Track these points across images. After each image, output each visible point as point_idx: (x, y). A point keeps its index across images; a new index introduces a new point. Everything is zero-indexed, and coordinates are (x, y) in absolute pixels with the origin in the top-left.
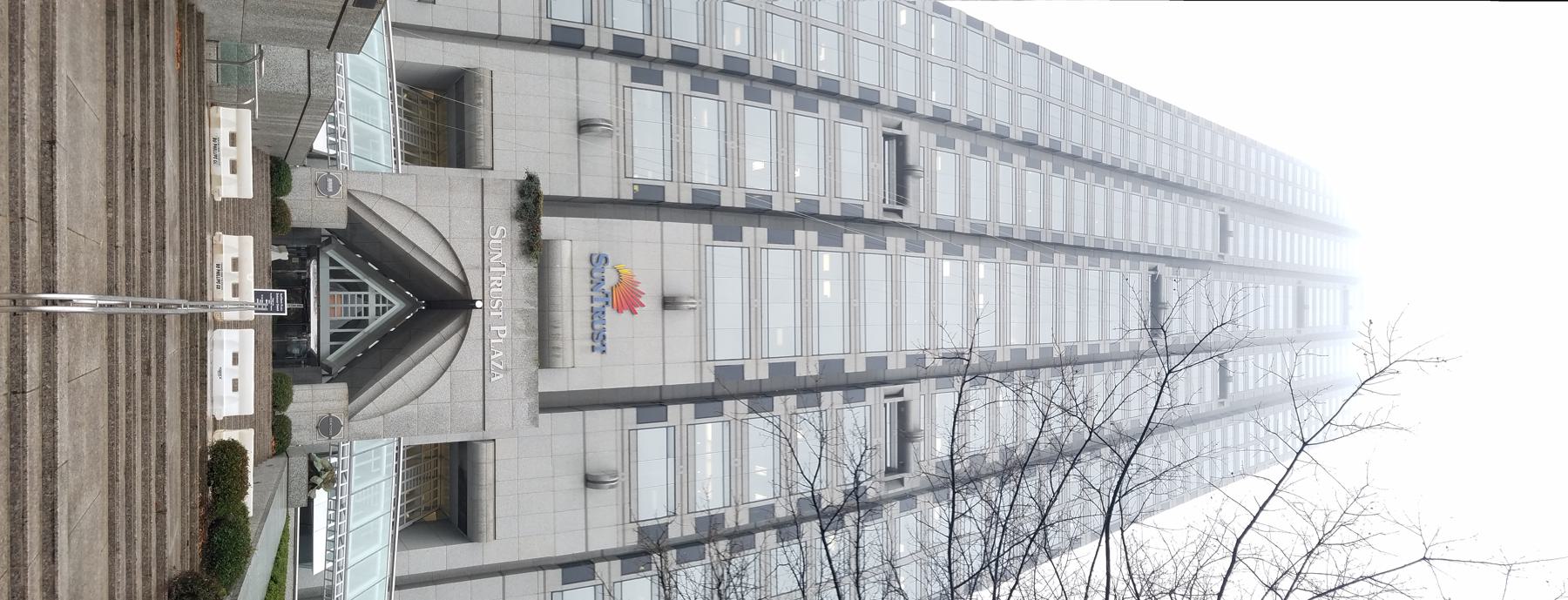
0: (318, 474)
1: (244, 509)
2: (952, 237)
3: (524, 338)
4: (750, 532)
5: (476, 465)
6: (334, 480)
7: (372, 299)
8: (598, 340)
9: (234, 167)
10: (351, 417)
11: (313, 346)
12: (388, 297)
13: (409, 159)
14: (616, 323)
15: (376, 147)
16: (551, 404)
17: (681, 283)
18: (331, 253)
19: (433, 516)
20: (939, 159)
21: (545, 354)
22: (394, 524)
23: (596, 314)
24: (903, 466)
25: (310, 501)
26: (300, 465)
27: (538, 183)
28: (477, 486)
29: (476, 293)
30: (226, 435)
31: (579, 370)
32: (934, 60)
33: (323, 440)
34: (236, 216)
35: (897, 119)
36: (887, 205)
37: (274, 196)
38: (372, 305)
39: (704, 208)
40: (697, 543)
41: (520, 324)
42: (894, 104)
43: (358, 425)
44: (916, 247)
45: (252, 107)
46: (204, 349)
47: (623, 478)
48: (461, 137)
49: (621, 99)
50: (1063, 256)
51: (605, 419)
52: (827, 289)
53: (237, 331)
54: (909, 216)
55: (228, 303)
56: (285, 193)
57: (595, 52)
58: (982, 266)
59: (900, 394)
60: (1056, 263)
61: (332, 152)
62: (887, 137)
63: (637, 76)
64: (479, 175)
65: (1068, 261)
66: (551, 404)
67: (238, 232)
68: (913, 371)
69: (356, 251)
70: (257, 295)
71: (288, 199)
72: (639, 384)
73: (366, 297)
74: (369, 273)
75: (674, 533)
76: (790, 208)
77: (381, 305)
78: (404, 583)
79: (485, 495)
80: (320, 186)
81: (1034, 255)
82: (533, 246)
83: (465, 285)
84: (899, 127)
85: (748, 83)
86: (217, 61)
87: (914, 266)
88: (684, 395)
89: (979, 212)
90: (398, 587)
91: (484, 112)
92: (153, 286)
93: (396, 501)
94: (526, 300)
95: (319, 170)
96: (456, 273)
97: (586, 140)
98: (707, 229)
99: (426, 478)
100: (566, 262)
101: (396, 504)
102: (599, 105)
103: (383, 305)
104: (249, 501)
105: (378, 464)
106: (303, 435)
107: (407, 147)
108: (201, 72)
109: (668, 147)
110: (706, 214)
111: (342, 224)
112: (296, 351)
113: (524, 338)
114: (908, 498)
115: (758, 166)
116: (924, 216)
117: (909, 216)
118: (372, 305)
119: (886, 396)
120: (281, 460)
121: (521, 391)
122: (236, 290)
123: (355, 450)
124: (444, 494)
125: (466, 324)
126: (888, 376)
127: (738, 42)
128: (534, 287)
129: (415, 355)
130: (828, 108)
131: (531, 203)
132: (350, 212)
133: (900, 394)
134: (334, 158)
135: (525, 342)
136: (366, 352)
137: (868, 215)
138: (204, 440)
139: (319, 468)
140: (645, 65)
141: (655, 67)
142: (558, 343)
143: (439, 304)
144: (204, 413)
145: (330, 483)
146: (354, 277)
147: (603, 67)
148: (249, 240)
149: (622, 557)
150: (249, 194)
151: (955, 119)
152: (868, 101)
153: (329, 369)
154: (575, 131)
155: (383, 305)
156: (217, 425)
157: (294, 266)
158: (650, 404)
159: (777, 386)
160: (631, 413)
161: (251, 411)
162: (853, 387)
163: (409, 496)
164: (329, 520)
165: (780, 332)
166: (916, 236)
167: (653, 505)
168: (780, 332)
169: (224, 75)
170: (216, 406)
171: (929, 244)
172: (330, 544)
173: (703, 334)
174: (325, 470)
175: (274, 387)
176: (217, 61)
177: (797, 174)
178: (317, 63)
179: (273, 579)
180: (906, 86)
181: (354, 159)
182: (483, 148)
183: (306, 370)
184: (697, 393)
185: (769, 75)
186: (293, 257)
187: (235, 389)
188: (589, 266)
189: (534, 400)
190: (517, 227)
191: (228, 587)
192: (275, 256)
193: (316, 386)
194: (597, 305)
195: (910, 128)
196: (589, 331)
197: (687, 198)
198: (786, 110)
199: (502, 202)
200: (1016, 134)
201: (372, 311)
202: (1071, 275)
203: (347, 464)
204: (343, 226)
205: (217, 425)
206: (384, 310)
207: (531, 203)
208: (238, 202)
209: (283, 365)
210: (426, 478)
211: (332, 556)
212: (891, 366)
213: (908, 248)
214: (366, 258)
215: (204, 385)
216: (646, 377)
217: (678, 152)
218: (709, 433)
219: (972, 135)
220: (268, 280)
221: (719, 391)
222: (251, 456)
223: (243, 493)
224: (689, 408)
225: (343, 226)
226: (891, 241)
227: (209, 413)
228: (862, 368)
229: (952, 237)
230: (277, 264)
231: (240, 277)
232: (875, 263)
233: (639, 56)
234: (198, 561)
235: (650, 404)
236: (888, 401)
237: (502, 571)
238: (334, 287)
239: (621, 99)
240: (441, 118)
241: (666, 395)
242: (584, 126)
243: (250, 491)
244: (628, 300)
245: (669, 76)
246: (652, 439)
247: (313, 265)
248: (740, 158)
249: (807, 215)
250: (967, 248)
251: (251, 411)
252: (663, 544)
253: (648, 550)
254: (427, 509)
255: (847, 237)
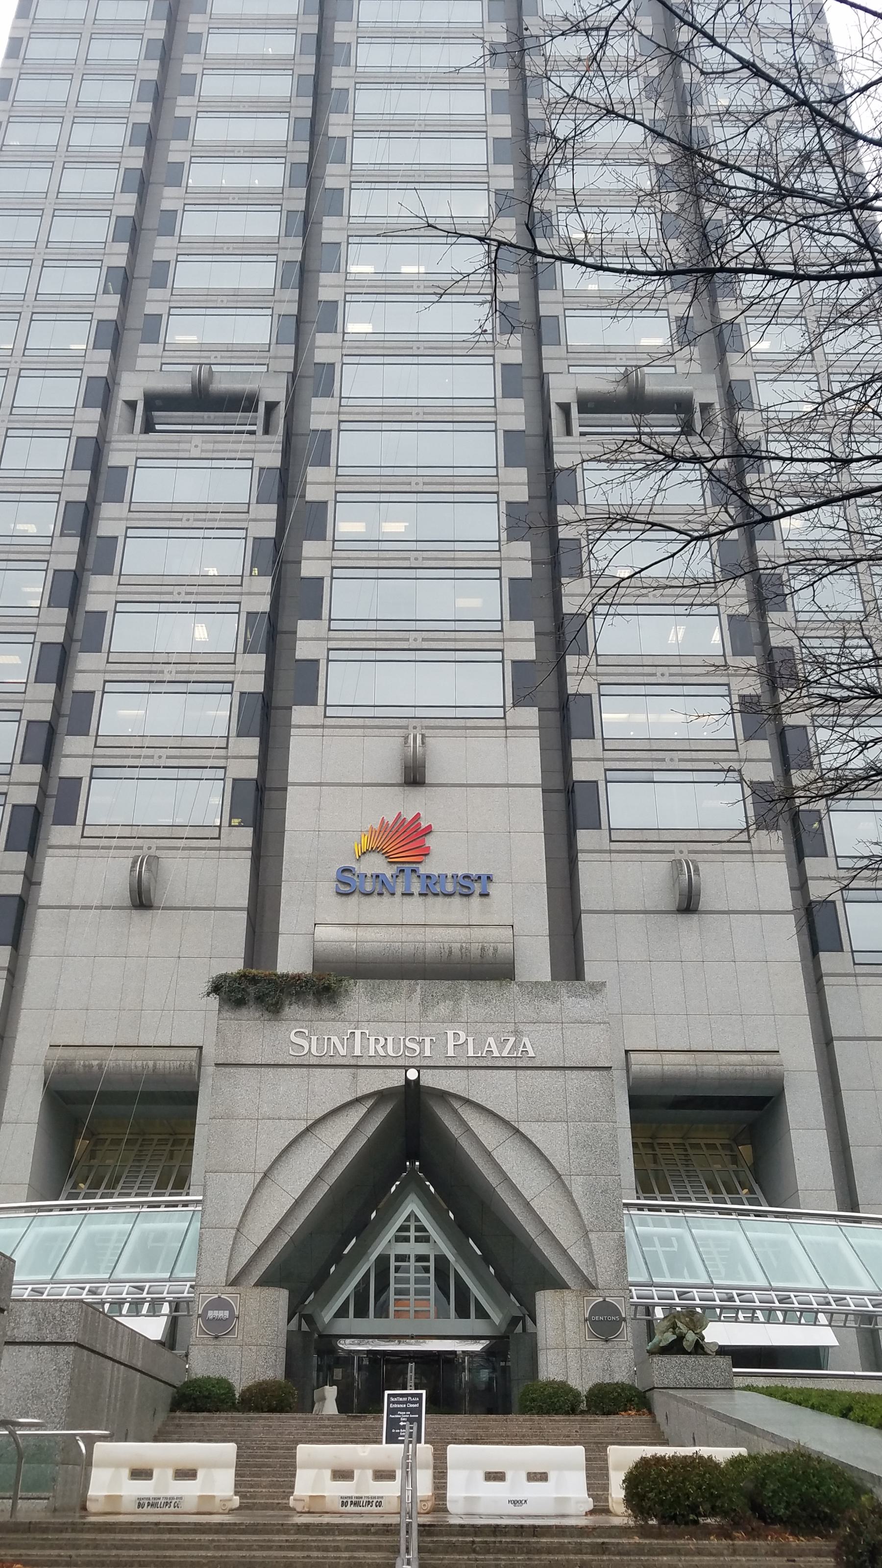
0: (679, 1337)
1: (736, 1462)
2: (307, 317)
3: (466, 1003)
4: (768, 653)
5: (665, 1081)
6: (690, 1312)
7: (402, 1248)
8: (472, 886)
9: (186, 1474)
10: (589, 1286)
11: (477, 1347)
12: (399, 1221)
13: (181, 1183)
14: (445, 858)
15: (161, 1236)
16: (569, 962)
17: (382, 755)
18: (327, 1315)
19: (745, 1151)
20: (180, 339)
21: (491, 971)
22: (758, 1214)
23: (432, 888)
24: (680, 405)
25: (723, 1351)
26: (666, 1370)
27: (224, 977)
28: (697, 1080)
29: (395, 1079)
30: (617, 1492)
31: (518, 918)
32: (20, 345)
33: (628, 1333)
34: (262, 1474)
35: (119, 409)
36: (259, 428)
37: (234, 1408)
38: (412, 1248)
39: (264, 721)
40: (781, 736)
41: (444, 1009)
42: (96, 413)
43: (604, 1276)
44: (325, 379)
45: (90, 1441)
46: (477, 1530)
47: (682, 852)
48: (150, 1097)
49: (101, 841)
50: (334, 118)
51: (595, 879)
52: (394, 528)
53: (451, 1474)
54: (275, 391)
55: (403, 1490)
56: (230, 1388)
57: (31, 879)
58: (353, 269)
59: (565, 408)
60: (346, 132)
61: (166, 1309)
62: (149, 427)
63: (67, 817)
64: (209, 1070)
65: (342, 109)
66: (569, 962)
67: (289, 1469)
68: (530, 386)
69: (324, 1274)
70: (392, 1439)
71: (240, 1383)
72: (542, 828)
73: (400, 1258)
74: (360, 1253)
75: (766, 773)
76: (266, 584)
77: (412, 1234)
78: (849, 1198)
79: (711, 1066)
80: (219, 1330)
81: (333, 176)
82: (323, 986)
83: (381, 1096)
84: (132, 405)
85: (77, 646)
86: (15, 1498)
87: (358, 382)
88: (557, 756)
89: (262, 275)
90: (855, 1207)
91: (114, 1060)
92: (384, 1539)
93: (722, 1211)
94: (406, 1000)
95: (194, 1329)
96: (362, 1110)
97: (161, 897)
98: (300, 714)
99: (687, 1161)
100: (348, 934)
101: (728, 1212)
102: (111, 874)
103: (413, 1229)
104: (722, 1454)
105: (665, 1241)
106: (618, 1363)
107: (161, 1186)
108: (30, 1527)
109: (173, 773)
110: (277, 716)
111: (280, 1297)
112: (484, 1375)
113: (466, 1003)
114: (735, 398)
115: (201, 633)
116: (275, 365)
117: (275, 391)
118: (412, 1248)
119: (569, 432)
120: (658, 1399)
121: (550, 1009)
122: (383, 1475)
123: (644, 1278)
124: (709, 1133)
125: (443, 1096)
126: (537, 429)
127: (15, 660)
128: (387, 986)
129: (492, 1179)
130: (110, 521)
131: (254, 989)
132: (264, 1282)
133: (565, 408)
134: (176, 1306)
135: (473, 1002)
136: (487, 1259)
137: (275, 460)
138: (624, 1531)
139: (670, 1337)
140: (51, 803)
141: (53, 789)
142: (475, 949)
143: (412, 1140)
144: (582, 1531)
145: (694, 1319)
146: (367, 1275)
147: (53, 867)
148: (303, 1451)
149: (800, 856)
150: (229, 1449)
151: (112, 314)
152: (93, 454)
153: (514, 1321)
154: (149, 913)
155: (413, 1229)
156: (601, 1509)
157: (348, 1376)
158: (570, 808)
159: (546, 607)
160: (585, 838)
161: (578, 1452)
162: (552, 485)
163: (715, 1190)
164: (753, 1320)
165: (462, 603)
166: (309, 379)
167: (722, 806)
168: (462, 603)
169: (37, 1485)
170: (571, 1509)
171: (320, 356)
172: (790, 1317)
173: (463, 723)
174: (674, 1326)
175: (541, 1411)
176: (15, 1498)
177: (213, 571)
178: (25, 1330)
179: (845, 1413)
180: (66, 392)
181: (178, 1274)
182: (169, 1061)
183: (515, 1361)
184: (555, 736)
185: (62, 614)
186: (333, 1377)
187: (543, 1477)
188: (354, 899)
189: (563, 988)
190: (291, 1010)
191: (859, 1491)
192: (330, 1407)
193: (541, 1344)
194: (416, 888)
195: (132, 387)
196: (457, 900)
197: (252, 745)
198: (114, 587)
199: (254, 1035)
200: (127, 204)
201: (422, 1249)
202: (367, 102)
203: (665, 1291)
204: (284, 1294)
205: (601, 1509)
206: (421, 1228)
207: (254, 989)
208: (244, 1468)
209: (507, 1396)
210: (687, 1161)
211: (807, 1316)
212: (519, 423)
213: (328, 393)
214: (336, 1257)
215: (535, 1531)
216: (530, 813)
217: (178, 758)
218: (617, 717)
219: (137, 284)
220: (369, 1420)
221: (553, 701)
222: (649, 1451)
223: (708, 1464)
224: (578, 747)
225: (284, 1294)
226: (317, 423)
227: (582, 1522)
228: (521, 474)
229: (307, 317)
230: (343, 1404)
231: (363, 1467)
232: (354, 449)
233: (37, 812)
234: (818, 1542)
235: (570, 808)
236: (576, 429)
237: (825, 1041)
238: (382, 1312)
239: (101, 841)
240: (117, 1130)
241: (557, 782)
242: (141, 900)
243: (705, 1451)
244: (407, 841)
245: (68, 768)
246: (627, 805)
247: (346, 1345)
248: (190, 660)
249: (277, 557)
250: (324, 294)
251: (578, 1452)
252: (780, 788)
253: (788, 813)
254: (735, 1160)
255: (312, 494)
